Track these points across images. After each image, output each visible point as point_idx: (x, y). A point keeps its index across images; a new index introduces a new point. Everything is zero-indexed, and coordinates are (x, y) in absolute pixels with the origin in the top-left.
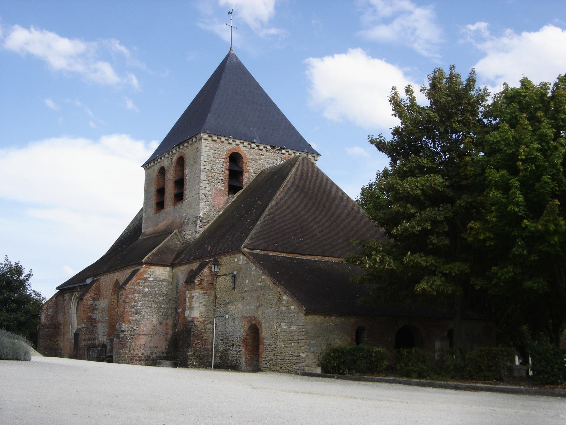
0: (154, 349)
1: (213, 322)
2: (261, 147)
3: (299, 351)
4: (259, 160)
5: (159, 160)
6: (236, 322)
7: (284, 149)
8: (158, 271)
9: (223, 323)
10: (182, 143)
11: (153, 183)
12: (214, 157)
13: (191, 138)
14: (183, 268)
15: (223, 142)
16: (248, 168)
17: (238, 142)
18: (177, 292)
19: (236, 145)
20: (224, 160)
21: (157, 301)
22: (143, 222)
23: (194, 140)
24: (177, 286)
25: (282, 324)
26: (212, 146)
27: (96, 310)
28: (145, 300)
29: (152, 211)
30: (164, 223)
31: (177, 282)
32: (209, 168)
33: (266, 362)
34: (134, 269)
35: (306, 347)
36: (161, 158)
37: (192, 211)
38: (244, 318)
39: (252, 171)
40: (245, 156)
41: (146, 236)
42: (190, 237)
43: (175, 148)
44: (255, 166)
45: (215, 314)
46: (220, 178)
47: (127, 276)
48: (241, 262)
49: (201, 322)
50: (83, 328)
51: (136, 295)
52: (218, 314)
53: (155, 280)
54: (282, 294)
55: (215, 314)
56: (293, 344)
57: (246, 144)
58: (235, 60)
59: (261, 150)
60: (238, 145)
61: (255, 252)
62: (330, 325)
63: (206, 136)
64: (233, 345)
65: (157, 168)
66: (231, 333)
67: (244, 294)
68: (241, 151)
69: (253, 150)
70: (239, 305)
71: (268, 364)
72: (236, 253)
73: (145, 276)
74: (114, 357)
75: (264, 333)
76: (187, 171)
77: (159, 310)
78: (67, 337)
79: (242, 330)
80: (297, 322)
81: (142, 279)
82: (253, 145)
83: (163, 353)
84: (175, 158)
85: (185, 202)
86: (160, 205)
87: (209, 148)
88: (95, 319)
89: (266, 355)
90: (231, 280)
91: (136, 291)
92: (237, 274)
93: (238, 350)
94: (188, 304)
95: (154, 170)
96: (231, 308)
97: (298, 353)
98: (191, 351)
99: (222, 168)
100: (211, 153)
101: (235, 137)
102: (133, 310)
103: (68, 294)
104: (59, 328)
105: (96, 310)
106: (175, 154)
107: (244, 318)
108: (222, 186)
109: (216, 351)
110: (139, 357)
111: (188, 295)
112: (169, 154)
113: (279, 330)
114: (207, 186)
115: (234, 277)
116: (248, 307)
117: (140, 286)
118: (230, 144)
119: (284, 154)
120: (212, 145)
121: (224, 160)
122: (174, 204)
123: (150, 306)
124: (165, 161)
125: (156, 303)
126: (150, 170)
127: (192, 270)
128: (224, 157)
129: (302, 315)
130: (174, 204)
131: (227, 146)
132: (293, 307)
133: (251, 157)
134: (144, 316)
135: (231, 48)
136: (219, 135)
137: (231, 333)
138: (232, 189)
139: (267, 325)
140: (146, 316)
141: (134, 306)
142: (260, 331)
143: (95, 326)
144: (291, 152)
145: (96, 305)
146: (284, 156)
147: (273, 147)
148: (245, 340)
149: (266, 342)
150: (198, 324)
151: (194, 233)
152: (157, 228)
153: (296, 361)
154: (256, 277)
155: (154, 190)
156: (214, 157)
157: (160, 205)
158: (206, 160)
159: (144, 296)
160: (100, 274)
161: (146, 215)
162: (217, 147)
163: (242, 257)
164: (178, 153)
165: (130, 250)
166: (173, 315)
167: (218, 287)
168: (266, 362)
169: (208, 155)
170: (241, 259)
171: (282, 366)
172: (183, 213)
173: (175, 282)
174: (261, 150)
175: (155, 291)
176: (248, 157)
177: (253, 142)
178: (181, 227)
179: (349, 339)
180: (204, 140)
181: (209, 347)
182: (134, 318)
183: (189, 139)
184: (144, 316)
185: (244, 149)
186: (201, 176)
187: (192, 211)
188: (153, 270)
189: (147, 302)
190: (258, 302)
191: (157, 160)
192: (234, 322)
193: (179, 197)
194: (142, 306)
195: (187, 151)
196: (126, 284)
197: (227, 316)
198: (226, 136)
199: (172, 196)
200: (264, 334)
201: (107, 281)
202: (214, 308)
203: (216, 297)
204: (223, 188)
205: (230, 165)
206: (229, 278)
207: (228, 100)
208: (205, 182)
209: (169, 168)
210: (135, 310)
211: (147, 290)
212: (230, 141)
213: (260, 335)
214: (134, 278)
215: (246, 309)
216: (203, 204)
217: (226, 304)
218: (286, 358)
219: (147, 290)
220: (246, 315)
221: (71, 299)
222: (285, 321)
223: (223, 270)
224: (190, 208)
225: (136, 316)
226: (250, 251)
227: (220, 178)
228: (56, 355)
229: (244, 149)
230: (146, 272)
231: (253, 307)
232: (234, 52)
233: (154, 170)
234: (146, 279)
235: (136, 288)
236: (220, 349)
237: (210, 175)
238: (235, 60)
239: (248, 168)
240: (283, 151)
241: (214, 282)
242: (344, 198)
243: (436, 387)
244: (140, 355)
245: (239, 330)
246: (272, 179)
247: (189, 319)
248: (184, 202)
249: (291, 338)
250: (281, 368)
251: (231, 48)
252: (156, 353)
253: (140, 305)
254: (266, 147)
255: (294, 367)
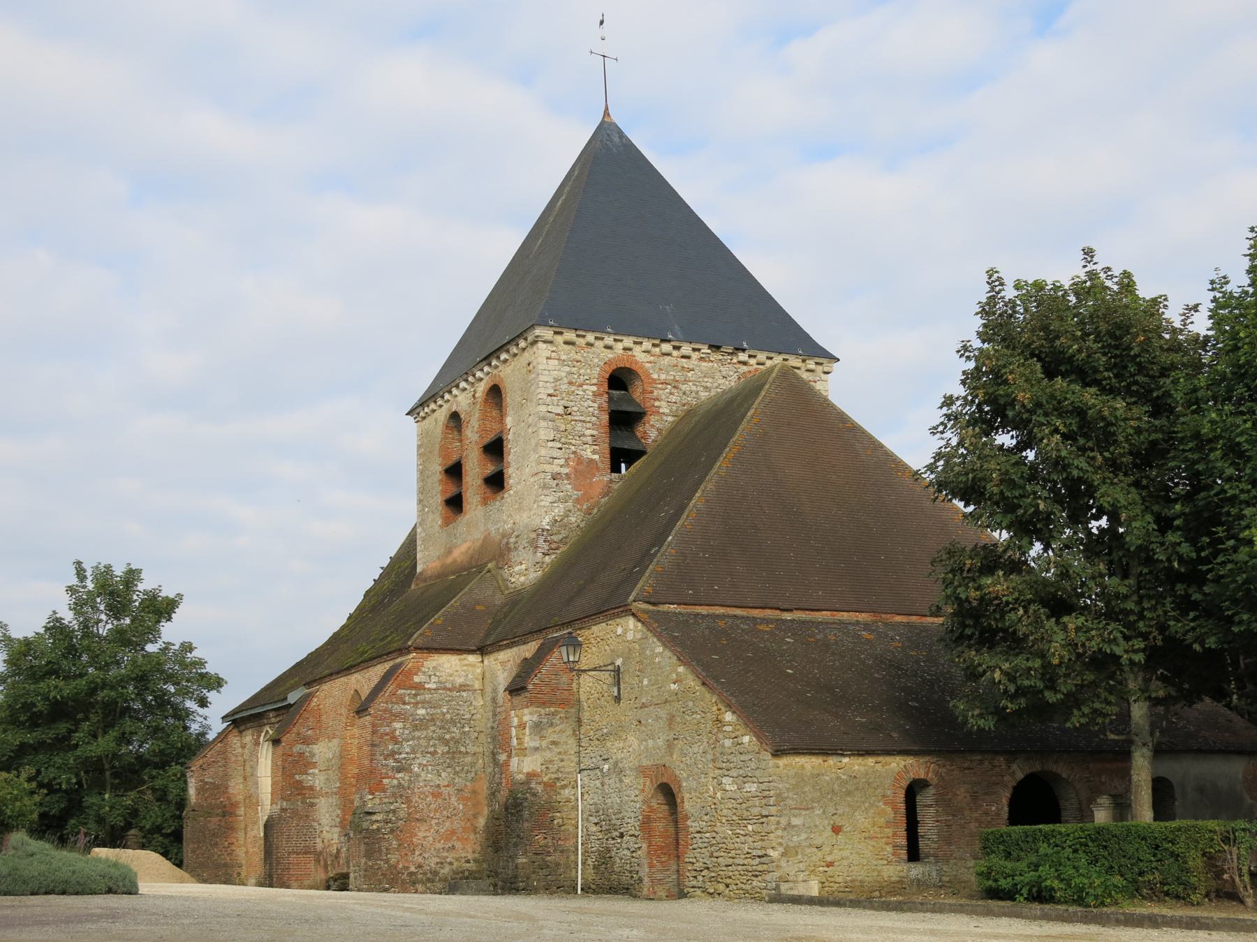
0: (445, 854)
1: (576, 781)
2: (686, 349)
3: (764, 844)
4: (684, 378)
5: (447, 396)
6: (627, 780)
7: (744, 350)
8: (447, 665)
9: (598, 783)
10: (495, 353)
11: (436, 452)
12: (570, 383)
13: (513, 340)
14: (503, 655)
15: (590, 345)
16: (657, 404)
17: (628, 341)
18: (495, 715)
19: (625, 349)
20: (594, 388)
21: (447, 737)
22: (419, 548)
23: (522, 344)
24: (494, 700)
25: (724, 780)
26: (564, 357)
27: (314, 765)
28: (419, 738)
29: (436, 519)
30: (464, 548)
31: (495, 691)
32: (560, 410)
33: (694, 874)
34: (391, 663)
35: (780, 833)
36: (450, 392)
37: (525, 516)
38: (642, 771)
39: (667, 411)
40: (649, 375)
41: (425, 580)
42: (522, 579)
43: (481, 365)
44: (673, 398)
45: (579, 763)
46: (588, 432)
47: (376, 680)
48: (630, 636)
49: (545, 784)
50: (283, 810)
51: (398, 725)
52: (587, 763)
53: (442, 687)
54: (723, 709)
55: (579, 763)
56: (750, 828)
57: (647, 344)
58: (616, 139)
59: (688, 357)
60: (630, 349)
61: (666, 607)
62: (838, 778)
63: (547, 333)
64: (622, 836)
65: (442, 415)
66: (616, 807)
67: (642, 714)
68: (637, 362)
69: (667, 358)
70: (633, 740)
71: (700, 878)
72: (618, 616)
73: (417, 679)
74: (352, 875)
75: (688, 804)
76: (509, 421)
77: (453, 758)
78: (253, 833)
79: (640, 798)
80: (757, 773)
81: (411, 688)
82: (666, 347)
83: (468, 862)
84: (482, 388)
85: (509, 495)
86: (455, 503)
87: (556, 362)
88: (311, 788)
89: (696, 856)
90: (610, 680)
91: (397, 716)
92: (623, 663)
93: (633, 846)
94: (515, 742)
95: (436, 421)
96: (614, 746)
97: (762, 848)
98: (525, 853)
99: (591, 407)
100: (556, 379)
101: (621, 330)
102: (391, 763)
103: (250, 731)
104: (233, 814)
105: (314, 765)
106: (481, 379)
107: (642, 771)
108: (594, 452)
109: (585, 852)
110: (411, 874)
111: (515, 721)
112: (466, 380)
113: (719, 795)
114: (556, 453)
115: (617, 671)
116: (650, 743)
117: (404, 703)
118: (608, 347)
119: (745, 363)
120: (566, 353)
121: (594, 388)
122: (485, 502)
123: (432, 749)
124: (460, 398)
125: (446, 743)
126: (426, 421)
127: (526, 659)
128: (595, 381)
129: (768, 756)
130: (485, 502)
131: (606, 351)
132: (746, 739)
133: (663, 377)
134: (418, 776)
135: (607, 108)
136: (580, 326)
137: (616, 807)
138: (620, 457)
139: (694, 784)
140: (423, 774)
141: (393, 753)
142: (679, 801)
143: (312, 805)
144: (762, 356)
145: (313, 755)
146: (745, 368)
147: (715, 348)
148: (646, 823)
149: (693, 825)
150: (540, 789)
151: (525, 571)
152: (449, 560)
153: (760, 868)
154: (666, 672)
155: (440, 469)
156: (570, 383)
157: (455, 503)
158: (551, 391)
159: (415, 728)
160: (320, 680)
161: (424, 530)
162: (578, 357)
163: (631, 622)
164: (486, 379)
165: (400, 614)
166: (490, 770)
167: (583, 697)
168: (694, 874)
169: (556, 380)
170: (629, 628)
171: (728, 881)
172: (505, 522)
173: (489, 689)
174: (688, 357)
175: (444, 714)
176: (655, 376)
177: (664, 341)
178: (502, 555)
179: (889, 809)
180: (545, 342)
181: (570, 843)
182: (395, 782)
183: (509, 343)
184: (418, 776)
185: (641, 354)
186: (542, 432)
187: (525, 516)
188: (434, 663)
189: (423, 742)
190: (670, 729)
191: (442, 397)
192: (621, 781)
193: (496, 482)
194: (413, 752)
195: (508, 371)
196: (373, 700)
197: (606, 767)
198: (597, 327)
199: (480, 482)
200: (687, 805)
201: (335, 694)
202: (576, 749)
203: (579, 721)
204: (596, 457)
205: (611, 400)
206: (607, 677)
207: (615, 239)
208: (550, 444)
209: (469, 414)
210: (397, 761)
211: (421, 712)
212: (609, 340)
213: (679, 809)
214: (391, 687)
215: (647, 749)
216: (550, 499)
217: (603, 739)
218: (737, 861)
219: (421, 712)
220: (645, 763)
221: (257, 744)
222: (730, 773)
223: (588, 658)
224: (520, 509)
225: (400, 775)
226: (651, 607)
227: (588, 432)
228: (228, 881)
229: (641, 354)
230: (417, 670)
231: (660, 742)
232: (615, 117)
233: (436, 421)
234: (419, 687)
235: (397, 708)
236: (595, 846)
237: (563, 427)
238: (616, 139)
239: (657, 404)
240: (743, 357)
241: (574, 685)
242: (888, 463)
243: (1072, 922)
244: (413, 869)
245: (632, 798)
246: (712, 425)
247: (521, 777)
248: (506, 495)
249: (746, 814)
250: (727, 886)
251: (607, 108)
252: (451, 864)
253: (408, 750)
254: (699, 350)
255: (754, 883)
